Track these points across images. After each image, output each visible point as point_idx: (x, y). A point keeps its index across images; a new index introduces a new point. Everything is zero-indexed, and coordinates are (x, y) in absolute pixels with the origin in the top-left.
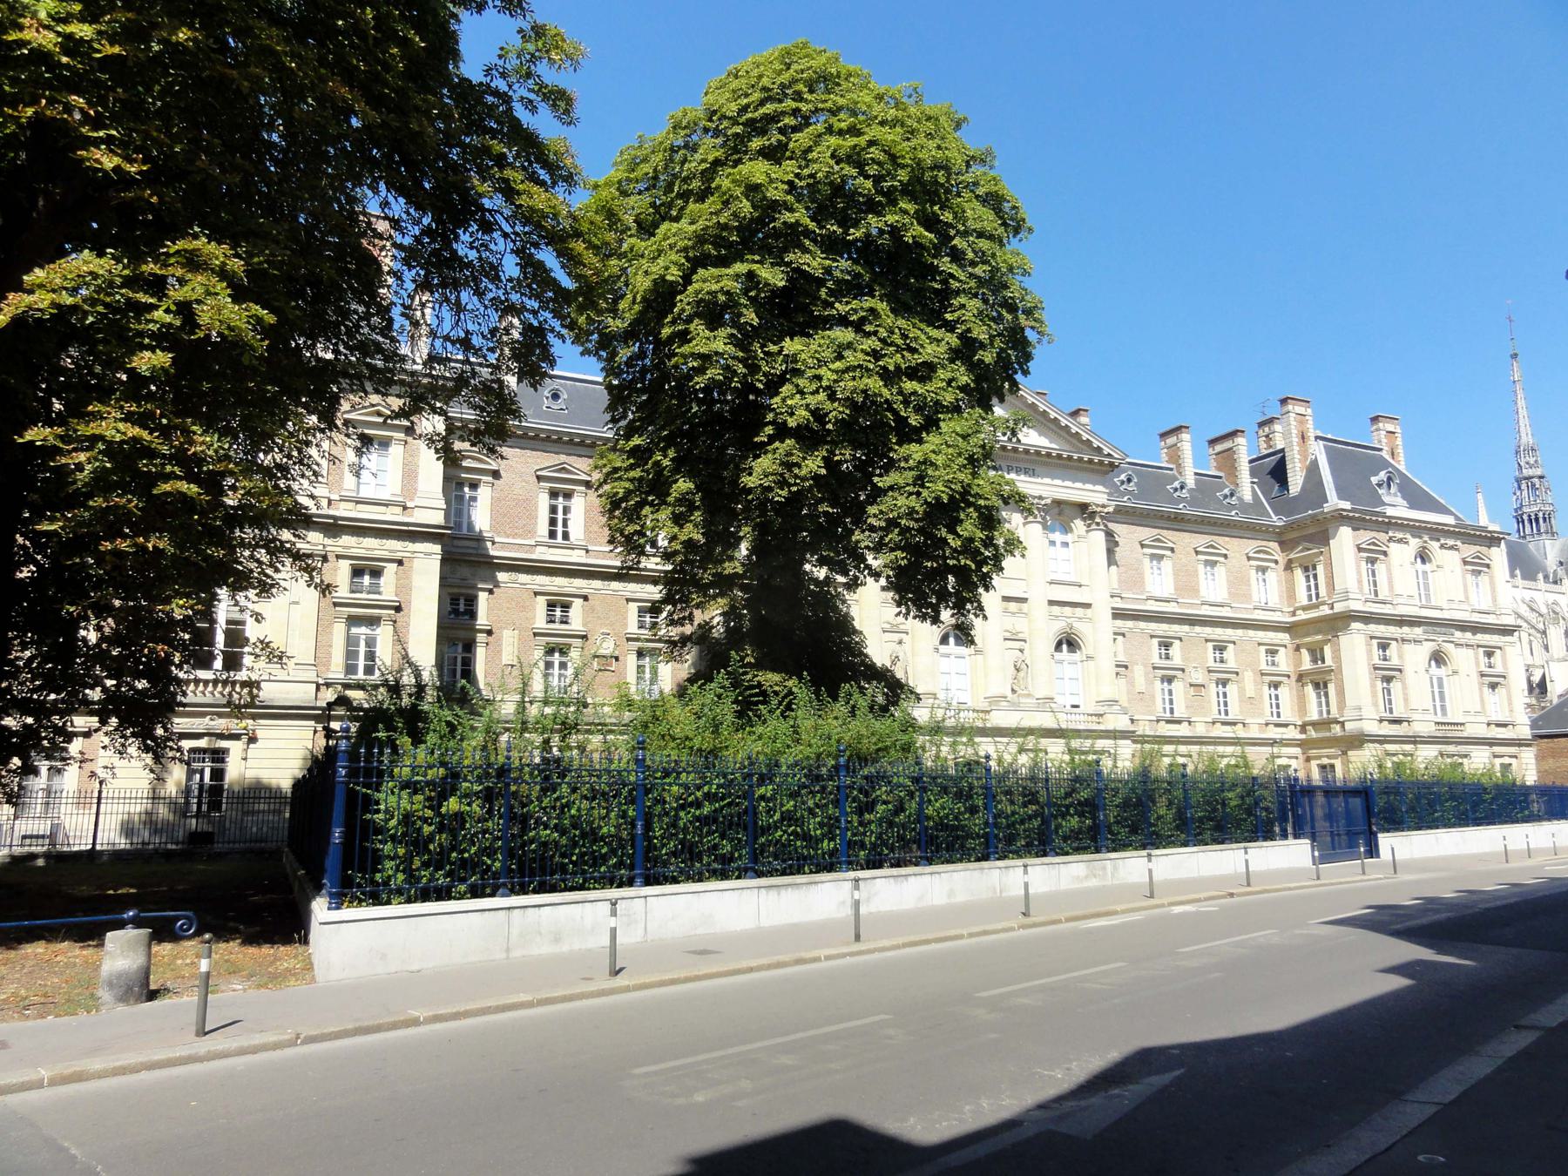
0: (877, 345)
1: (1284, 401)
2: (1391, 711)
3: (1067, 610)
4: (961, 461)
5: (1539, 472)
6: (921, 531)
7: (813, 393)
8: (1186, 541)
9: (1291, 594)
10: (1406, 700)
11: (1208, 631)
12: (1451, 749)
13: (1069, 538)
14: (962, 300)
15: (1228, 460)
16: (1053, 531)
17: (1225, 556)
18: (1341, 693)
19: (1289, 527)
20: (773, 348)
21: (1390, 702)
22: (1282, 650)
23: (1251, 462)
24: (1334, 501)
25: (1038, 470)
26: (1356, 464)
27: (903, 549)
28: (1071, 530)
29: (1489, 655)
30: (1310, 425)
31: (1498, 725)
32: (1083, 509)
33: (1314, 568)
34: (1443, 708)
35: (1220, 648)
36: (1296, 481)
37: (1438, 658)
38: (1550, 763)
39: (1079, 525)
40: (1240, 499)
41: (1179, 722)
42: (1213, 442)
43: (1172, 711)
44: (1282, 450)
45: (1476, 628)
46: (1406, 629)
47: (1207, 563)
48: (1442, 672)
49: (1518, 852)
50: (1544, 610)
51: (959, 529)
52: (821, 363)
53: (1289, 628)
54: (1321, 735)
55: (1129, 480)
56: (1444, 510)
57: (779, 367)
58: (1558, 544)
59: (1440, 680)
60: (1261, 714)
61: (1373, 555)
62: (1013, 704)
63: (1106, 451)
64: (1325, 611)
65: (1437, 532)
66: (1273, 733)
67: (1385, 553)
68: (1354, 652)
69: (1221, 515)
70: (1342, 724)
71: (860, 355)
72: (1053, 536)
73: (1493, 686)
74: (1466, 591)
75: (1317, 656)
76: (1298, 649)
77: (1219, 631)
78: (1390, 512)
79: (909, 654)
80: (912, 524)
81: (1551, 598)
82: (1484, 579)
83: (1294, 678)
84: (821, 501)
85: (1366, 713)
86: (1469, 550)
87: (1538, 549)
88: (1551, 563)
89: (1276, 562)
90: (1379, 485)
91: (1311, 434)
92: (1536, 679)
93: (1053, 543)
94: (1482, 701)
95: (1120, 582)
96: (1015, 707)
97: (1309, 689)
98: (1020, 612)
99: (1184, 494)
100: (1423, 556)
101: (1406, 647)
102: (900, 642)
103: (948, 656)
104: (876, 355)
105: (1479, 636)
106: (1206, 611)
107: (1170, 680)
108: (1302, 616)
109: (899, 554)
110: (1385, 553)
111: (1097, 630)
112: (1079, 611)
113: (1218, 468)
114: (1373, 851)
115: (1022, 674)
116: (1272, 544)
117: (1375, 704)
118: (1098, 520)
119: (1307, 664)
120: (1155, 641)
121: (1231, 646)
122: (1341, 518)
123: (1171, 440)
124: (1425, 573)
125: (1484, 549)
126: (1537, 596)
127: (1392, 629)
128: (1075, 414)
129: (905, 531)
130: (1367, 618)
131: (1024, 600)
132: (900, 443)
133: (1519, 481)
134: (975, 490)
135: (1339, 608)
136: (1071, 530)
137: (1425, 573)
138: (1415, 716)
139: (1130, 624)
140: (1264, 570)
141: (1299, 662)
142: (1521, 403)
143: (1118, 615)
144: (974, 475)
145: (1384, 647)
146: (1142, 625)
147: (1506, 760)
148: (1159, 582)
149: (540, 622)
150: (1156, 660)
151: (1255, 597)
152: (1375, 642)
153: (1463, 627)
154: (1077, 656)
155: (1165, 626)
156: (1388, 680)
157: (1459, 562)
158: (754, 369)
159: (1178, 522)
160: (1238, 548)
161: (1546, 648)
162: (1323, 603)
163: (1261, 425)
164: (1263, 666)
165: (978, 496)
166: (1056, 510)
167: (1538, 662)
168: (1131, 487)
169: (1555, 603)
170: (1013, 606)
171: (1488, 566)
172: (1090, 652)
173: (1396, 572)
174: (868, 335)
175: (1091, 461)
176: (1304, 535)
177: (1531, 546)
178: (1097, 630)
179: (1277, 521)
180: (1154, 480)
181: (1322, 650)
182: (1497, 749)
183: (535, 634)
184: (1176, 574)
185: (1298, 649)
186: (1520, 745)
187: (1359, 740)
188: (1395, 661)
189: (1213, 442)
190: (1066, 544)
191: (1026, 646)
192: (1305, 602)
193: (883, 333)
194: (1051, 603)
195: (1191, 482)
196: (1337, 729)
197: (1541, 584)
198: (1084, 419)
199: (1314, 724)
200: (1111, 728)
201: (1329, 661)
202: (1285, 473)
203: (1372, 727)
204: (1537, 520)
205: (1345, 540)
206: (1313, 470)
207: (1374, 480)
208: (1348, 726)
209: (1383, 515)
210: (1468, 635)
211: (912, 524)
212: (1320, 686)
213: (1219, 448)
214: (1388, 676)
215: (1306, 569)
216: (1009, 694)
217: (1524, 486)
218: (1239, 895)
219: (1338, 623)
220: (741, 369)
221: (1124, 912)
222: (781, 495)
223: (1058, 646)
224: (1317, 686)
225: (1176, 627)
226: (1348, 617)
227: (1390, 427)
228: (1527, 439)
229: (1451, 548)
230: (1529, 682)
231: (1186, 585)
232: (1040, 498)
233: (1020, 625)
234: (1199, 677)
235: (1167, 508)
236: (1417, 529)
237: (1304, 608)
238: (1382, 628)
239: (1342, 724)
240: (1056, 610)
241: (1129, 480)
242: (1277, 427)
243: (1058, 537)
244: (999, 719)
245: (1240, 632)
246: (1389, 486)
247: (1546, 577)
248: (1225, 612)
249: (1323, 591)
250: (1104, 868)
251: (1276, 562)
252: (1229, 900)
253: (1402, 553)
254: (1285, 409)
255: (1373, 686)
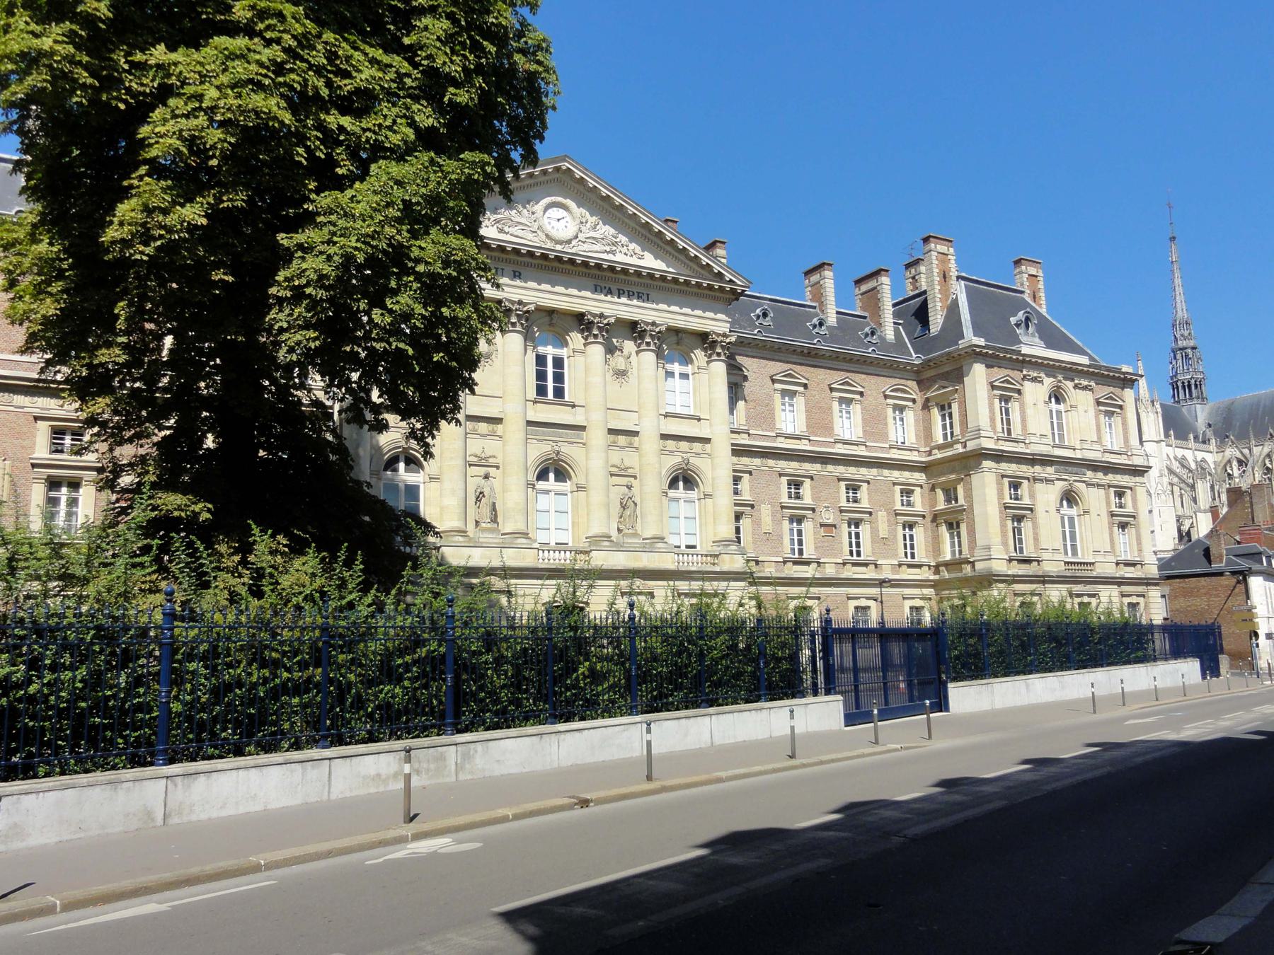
0: (281, 56)
1: (926, 240)
2: (1021, 550)
3: (684, 445)
4: (393, 212)
5: (1192, 343)
6: (331, 300)
7: (187, 116)
8: (821, 377)
9: (927, 432)
10: (1036, 539)
11: (840, 470)
12: (1077, 588)
13: (689, 369)
14: (427, 21)
15: (872, 299)
16: (672, 362)
17: (861, 394)
18: (972, 532)
19: (926, 365)
20: (139, 57)
21: (1021, 541)
22: (918, 489)
23: (894, 305)
24: (971, 338)
25: (653, 295)
26: (995, 304)
27: (314, 327)
28: (691, 362)
29: (1120, 495)
30: (953, 265)
31: (1127, 564)
32: (704, 340)
33: (950, 407)
34: (1074, 547)
35: (853, 488)
36: (937, 320)
37: (1069, 498)
38: (1181, 603)
39: (699, 356)
40: (882, 339)
41: (807, 563)
42: (858, 282)
43: (801, 552)
44: (925, 292)
45: (1108, 468)
46: (1038, 468)
47: (841, 400)
48: (1073, 512)
49: (1110, 698)
50: (1193, 466)
51: (388, 302)
52: (203, 78)
53: (924, 468)
54: (953, 575)
55: (765, 315)
56: (1081, 351)
57: (150, 83)
58: (1207, 408)
59: (1071, 520)
60: (895, 555)
61: (1006, 395)
62: (617, 544)
63: (728, 276)
64: (959, 449)
65: (1071, 371)
66: (907, 574)
67: (1019, 392)
68: (986, 489)
69: (858, 351)
70: (973, 563)
71: (254, 67)
72: (669, 367)
73: (1123, 526)
74: (1099, 430)
75: (951, 495)
76: (933, 489)
77: (852, 470)
78: (1025, 350)
79: (498, 489)
80: (321, 294)
81: (1200, 455)
82: (1117, 420)
83: (929, 518)
84: (216, 265)
85: (994, 554)
86: (1103, 391)
87: (1189, 411)
88: (1201, 424)
89: (914, 401)
90: (1018, 325)
91: (954, 273)
92: (1185, 528)
93: (670, 374)
94: (1112, 540)
95: (747, 417)
96: (619, 547)
97: (943, 529)
98: (631, 445)
99: (823, 330)
100: (1057, 396)
101: (1039, 486)
102: (486, 477)
103: (547, 492)
104: (279, 69)
105: (1110, 476)
106: (840, 449)
107: (800, 520)
108: (938, 455)
109: (313, 334)
110: (1019, 392)
111: (716, 467)
112: (697, 446)
113: (863, 309)
114: (941, 704)
115: (628, 512)
116: (909, 383)
117: (1005, 544)
118: (719, 350)
119: (941, 505)
120: (784, 480)
121: (865, 485)
122: (975, 354)
123: (815, 278)
124: (1059, 413)
125: (1117, 391)
126: (1189, 455)
127: (1024, 468)
128: (711, 246)
129: (314, 304)
130: (999, 457)
131: (636, 434)
132: (318, 191)
133: (1174, 351)
134: (415, 253)
135: (971, 445)
136: (691, 362)
137: (1059, 413)
138: (1045, 556)
139: (757, 461)
140: (901, 409)
141: (933, 502)
142: (1178, 281)
143: (738, 451)
144: (414, 235)
145: (1015, 486)
146: (771, 462)
147: (1134, 600)
148: (791, 419)
149: (42, 451)
150: (785, 499)
151: (892, 437)
152: (1006, 481)
153: (1095, 466)
154: (693, 494)
155: (794, 465)
156: (1019, 519)
157: (1092, 402)
158: (110, 82)
159: (811, 357)
160: (874, 386)
161: (1195, 500)
162: (957, 442)
163: (908, 266)
164: (898, 506)
165: (418, 261)
166: (674, 339)
167: (1188, 512)
168: (767, 322)
169: (1204, 460)
170: (622, 440)
171: (1121, 407)
172: (709, 490)
173: (1030, 411)
174: (268, 43)
175: (710, 287)
176: (939, 373)
177: (1184, 410)
178: (716, 467)
179: (915, 358)
180: (791, 315)
181: (955, 489)
182: (1126, 589)
183: (34, 466)
184: (808, 411)
185: (933, 489)
186: (1148, 584)
187: (989, 579)
188: (1026, 501)
189: (858, 282)
190: (684, 376)
191: (635, 483)
192: (941, 441)
193: (288, 40)
194: (665, 437)
195: (832, 320)
196: (967, 569)
197: (1192, 444)
198: (720, 251)
199: (947, 565)
200: (725, 568)
201: (961, 501)
202: (927, 309)
203: (1000, 567)
204: (1189, 386)
205: (978, 375)
206: (953, 309)
207: (1013, 320)
208: (979, 566)
209: (1019, 353)
210: (1100, 475)
211: (321, 294)
212: (953, 526)
213: (864, 288)
214: (1018, 516)
215: (942, 408)
216: (614, 533)
217: (1179, 356)
218: (600, 802)
219: (971, 461)
220: (84, 77)
221: (270, 866)
222: (143, 252)
223: (673, 484)
224: (950, 526)
225: (807, 466)
226: (982, 454)
227: (1033, 271)
228: (1182, 313)
229: (1085, 388)
230: (1179, 531)
231: (819, 421)
232: (654, 324)
233: (630, 459)
234: (829, 517)
235: (800, 342)
236: (1051, 368)
237: (940, 447)
238: (1014, 466)
239: (973, 563)
240: (671, 444)
241: (765, 315)
242: (923, 269)
243: (676, 368)
244: (601, 559)
245: (874, 471)
246: (1027, 327)
247: (1196, 438)
248: (861, 451)
249: (957, 430)
250: (442, 758)
251: (914, 401)
252: (579, 812)
253: (1036, 392)
254: (927, 248)
255: (1003, 526)
